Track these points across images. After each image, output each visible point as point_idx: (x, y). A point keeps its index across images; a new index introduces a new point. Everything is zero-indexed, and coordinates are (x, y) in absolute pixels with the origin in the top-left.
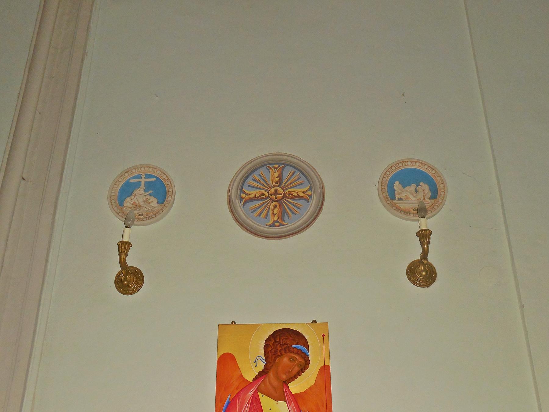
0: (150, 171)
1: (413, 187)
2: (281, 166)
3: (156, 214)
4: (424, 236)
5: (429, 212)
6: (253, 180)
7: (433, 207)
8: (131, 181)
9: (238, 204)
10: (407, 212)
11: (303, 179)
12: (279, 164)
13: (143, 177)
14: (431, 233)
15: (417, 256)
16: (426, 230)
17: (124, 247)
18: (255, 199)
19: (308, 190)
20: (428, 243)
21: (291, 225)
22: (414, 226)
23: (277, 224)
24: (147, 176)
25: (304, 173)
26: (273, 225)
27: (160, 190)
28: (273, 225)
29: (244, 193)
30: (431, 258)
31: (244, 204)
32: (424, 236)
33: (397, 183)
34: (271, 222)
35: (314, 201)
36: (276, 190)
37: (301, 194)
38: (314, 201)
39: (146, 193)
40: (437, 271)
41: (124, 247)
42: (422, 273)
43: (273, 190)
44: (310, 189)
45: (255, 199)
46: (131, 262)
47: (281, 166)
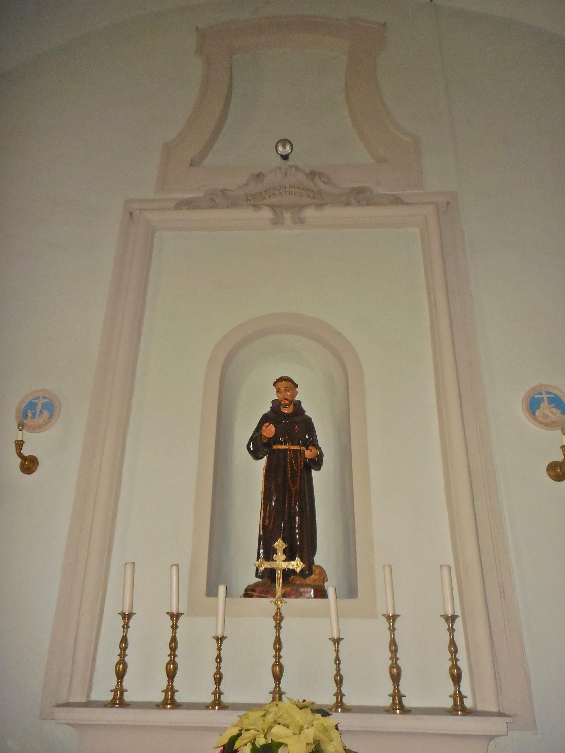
24: (44, 398)
41: (19, 445)
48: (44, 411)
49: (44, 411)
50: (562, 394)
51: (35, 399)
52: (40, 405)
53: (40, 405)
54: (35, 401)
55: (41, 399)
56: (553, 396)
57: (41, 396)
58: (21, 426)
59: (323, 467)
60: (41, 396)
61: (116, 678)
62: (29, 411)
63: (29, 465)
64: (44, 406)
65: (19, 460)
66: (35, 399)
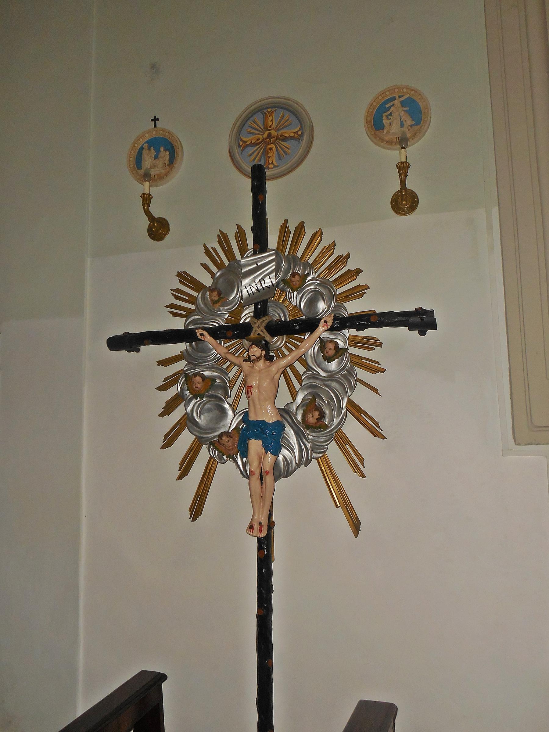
1: (396, 116)
5: (411, 140)
6: (253, 122)
7: (414, 135)
9: (237, 151)
10: (390, 143)
12: (264, 109)
14: (409, 166)
16: (406, 162)
17: (147, 199)
18: (252, 145)
19: (299, 130)
20: (406, 175)
22: (396, 155)
29: (241, 140)
30: (408, 186)
31: (243, 150)
32: (403, 169)
33: (252, 308)
41: (147, 199)
44: (301, 129)
45: (252, 145)
46: (157, 211)
65: (398, 187)
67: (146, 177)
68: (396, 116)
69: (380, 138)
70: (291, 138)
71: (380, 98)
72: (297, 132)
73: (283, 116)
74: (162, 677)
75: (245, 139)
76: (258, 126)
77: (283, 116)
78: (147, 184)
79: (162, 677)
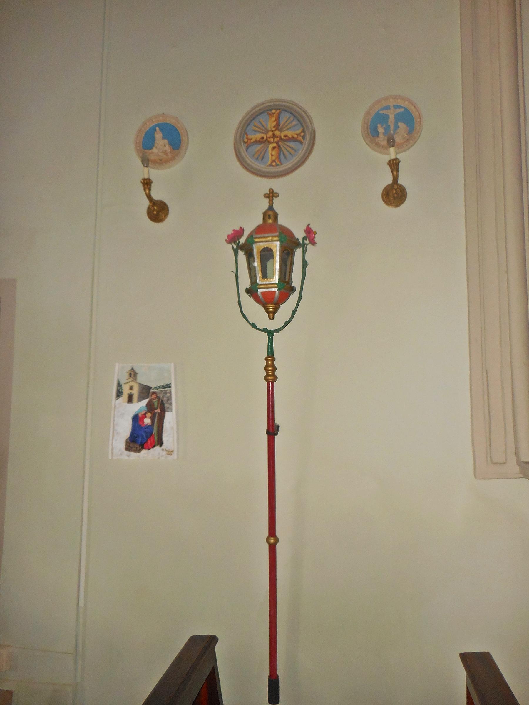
0: (400, 102)
1: (391, 126)
2: (278, 111)
3: (167, 161)
4: (394, 165)
8: (381, 112)
11: (295, 122)
12: (276, 109)
13: (392, 108)
15: (389, 180)
17: (147, 183)
19: (302, 132)
21: (287, 165)
23: (274, 164)
24: (396, 107)
25: (299, 116)
26: (271, 165)
27: (175, 138)
28: (271, 165)
30: (400, 182)
32: (394, 165)
34: (269, 163)
35: (306, 143)
36: (274, 134)
37: (295, 136)
38: (306, 143)
39: (163, 140)
40: (155, 223)
41: (147, 183)
42: (395, 195)
43: (270, 134)
44: (303, 131)
45: (256, 142)
46: (156, 196)
47: (278, 111)
48: (400, 124)
49: (400, 124)
50: (419, 120)
51: (383, 109)
52: (392, 117)
53: (392, 117)
54: (385, 112)
55: (392, 109)
56: (402, 110)
57: (392, 105)
58: (146, 162)
59: (133, 455)
60: (392, 105)
61: (277, 546)
62: (379, 125)
63: (158, 211)
64: (399, 118)
65: (147, 203)
66: (383, 109)
67: (391, 142)
68: (391, 126)
69: (382, 147)
70: (292, 139)
71: (138, 142)
72: (300, 134)
73: (289, 118)
74: (212, 640)
75: (250, 136)
76: (258, 128)
77: (289, 118)
78: (392, 150)
79: (212, 640)
